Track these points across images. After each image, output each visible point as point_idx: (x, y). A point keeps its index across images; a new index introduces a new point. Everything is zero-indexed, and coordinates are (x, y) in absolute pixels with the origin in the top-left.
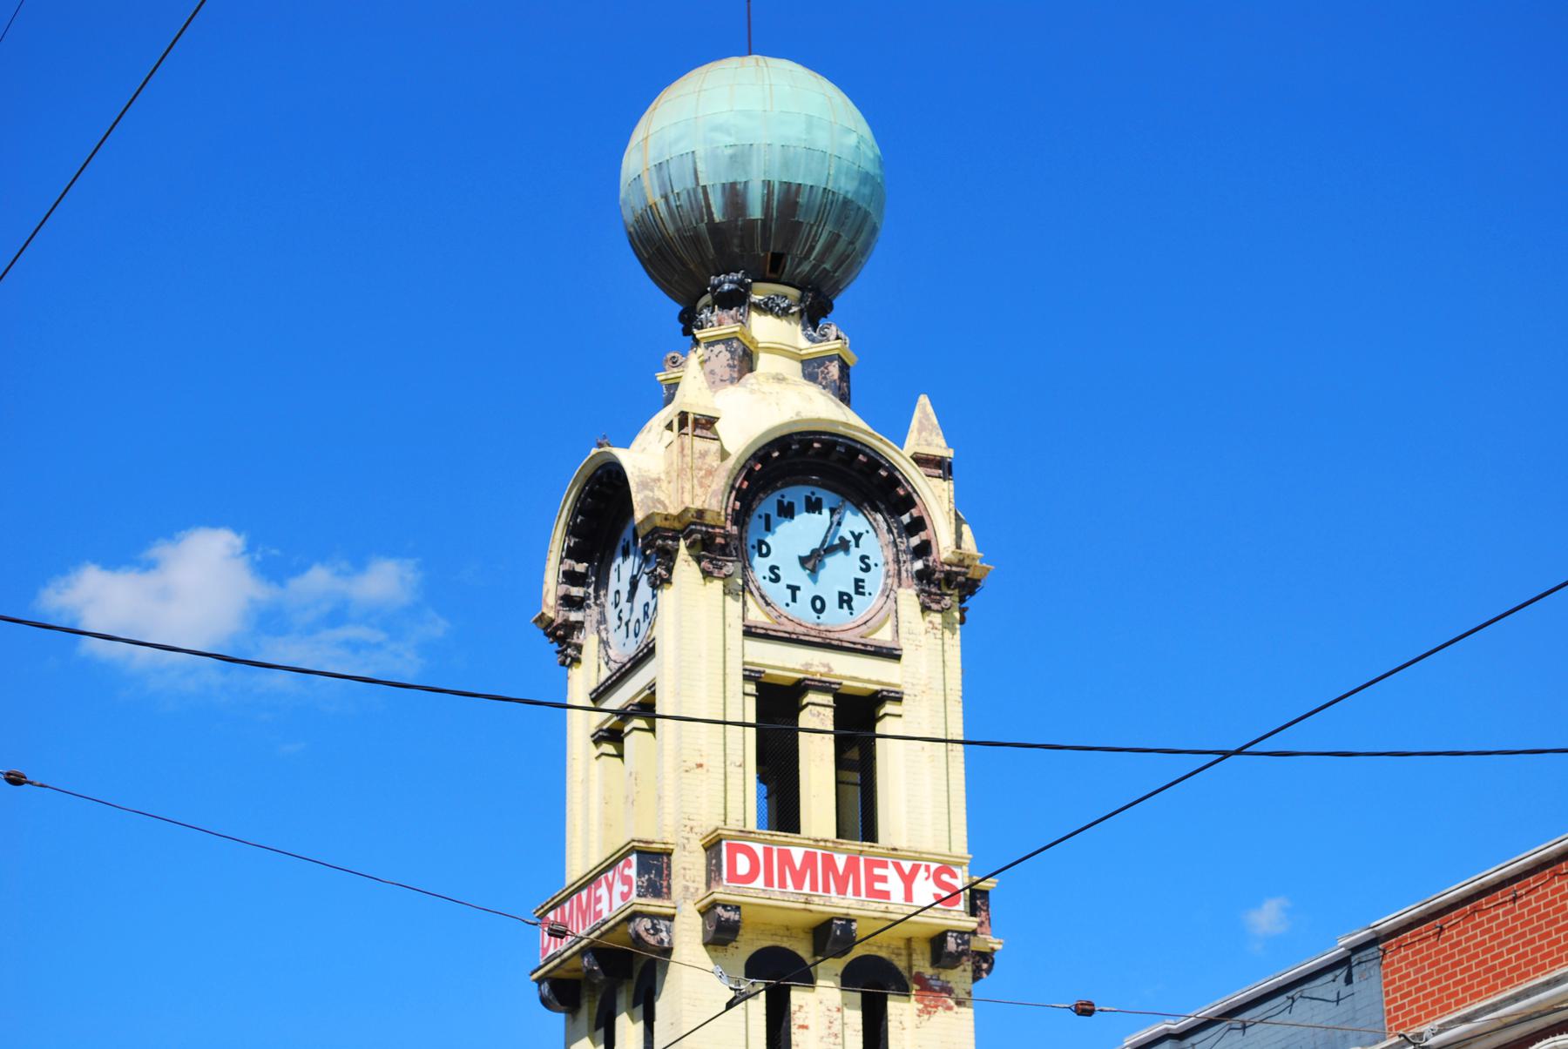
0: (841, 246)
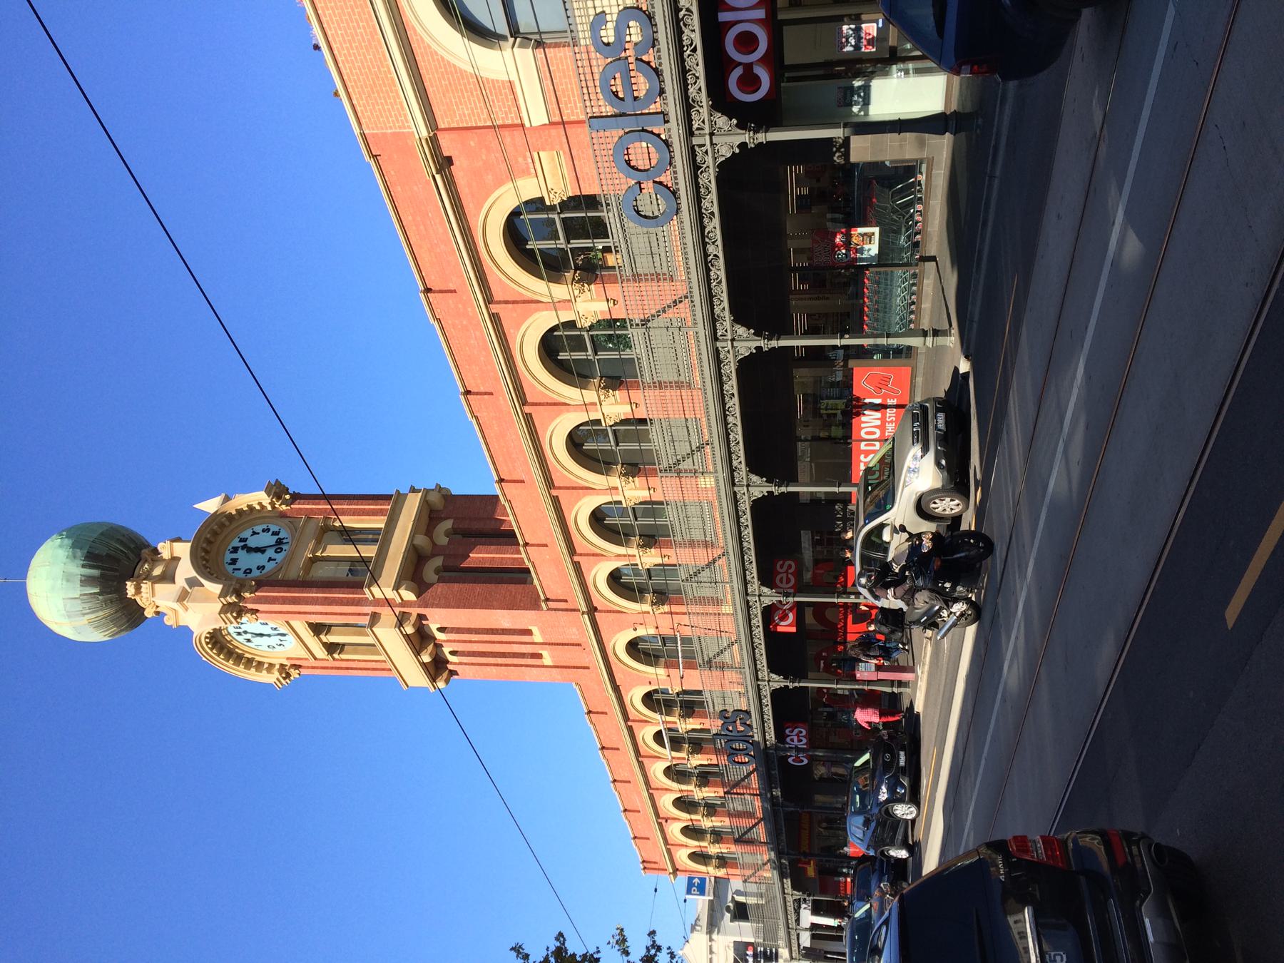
0: (124, 540)
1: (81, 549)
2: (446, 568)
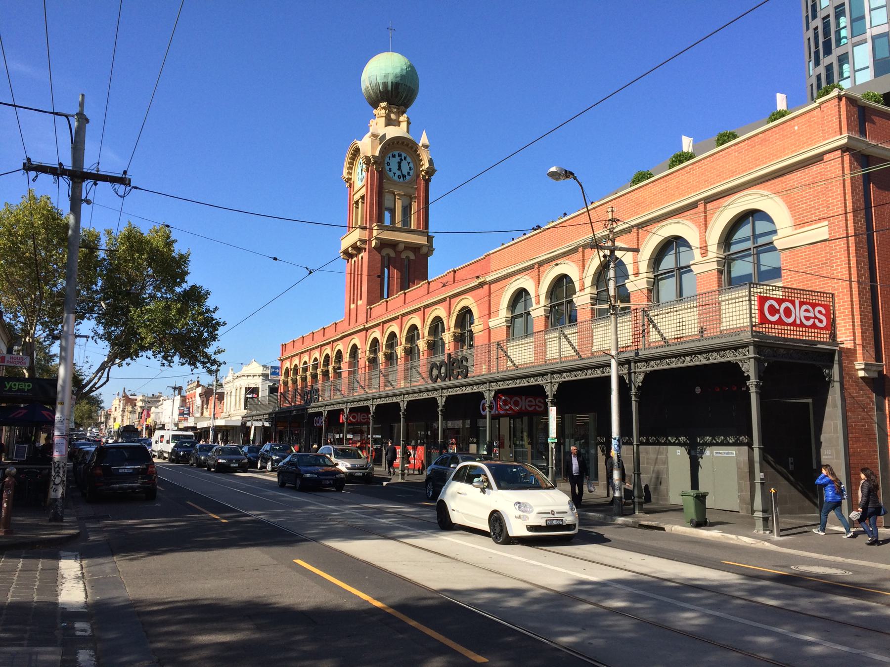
1: (401, 80)
2: (389, 258)
